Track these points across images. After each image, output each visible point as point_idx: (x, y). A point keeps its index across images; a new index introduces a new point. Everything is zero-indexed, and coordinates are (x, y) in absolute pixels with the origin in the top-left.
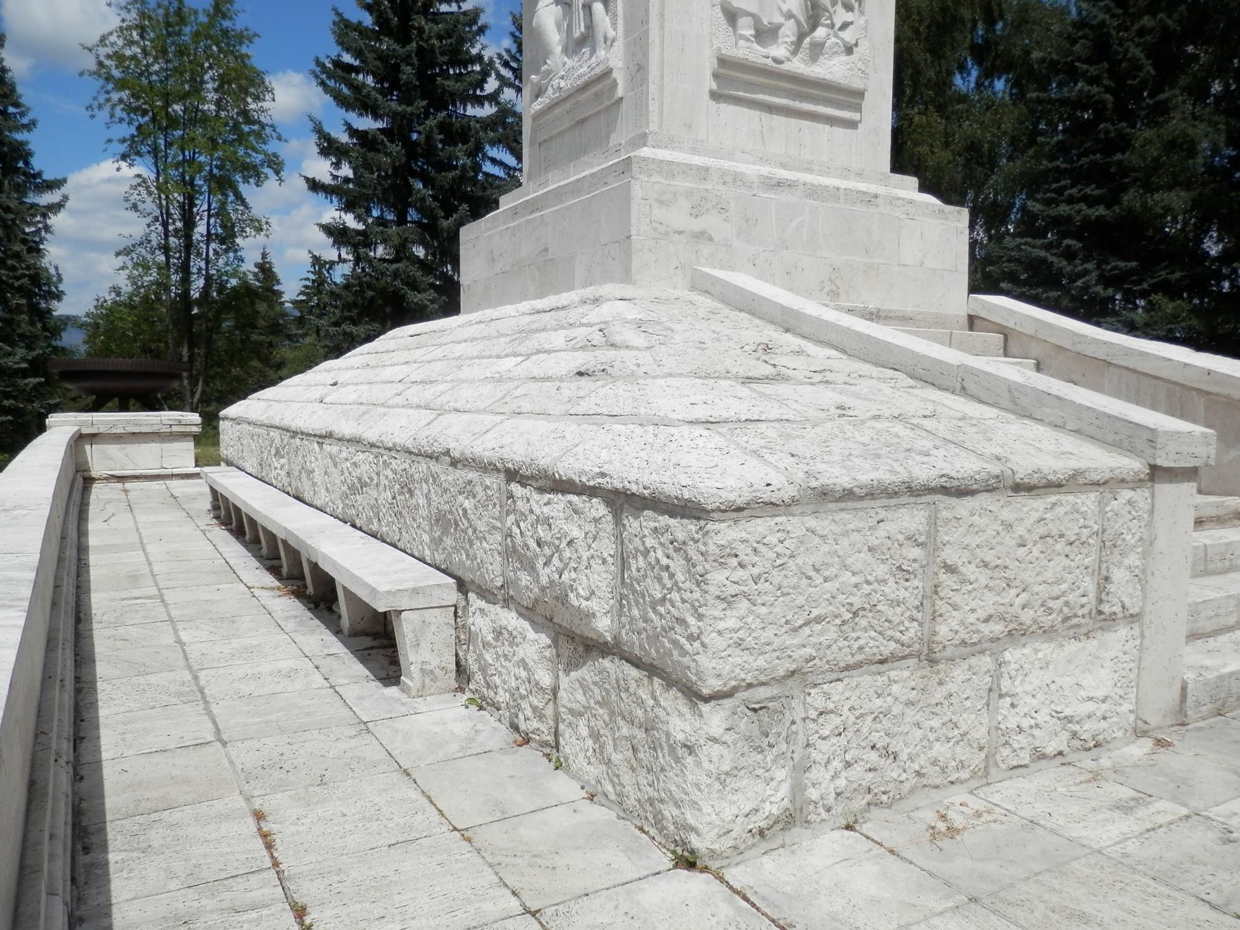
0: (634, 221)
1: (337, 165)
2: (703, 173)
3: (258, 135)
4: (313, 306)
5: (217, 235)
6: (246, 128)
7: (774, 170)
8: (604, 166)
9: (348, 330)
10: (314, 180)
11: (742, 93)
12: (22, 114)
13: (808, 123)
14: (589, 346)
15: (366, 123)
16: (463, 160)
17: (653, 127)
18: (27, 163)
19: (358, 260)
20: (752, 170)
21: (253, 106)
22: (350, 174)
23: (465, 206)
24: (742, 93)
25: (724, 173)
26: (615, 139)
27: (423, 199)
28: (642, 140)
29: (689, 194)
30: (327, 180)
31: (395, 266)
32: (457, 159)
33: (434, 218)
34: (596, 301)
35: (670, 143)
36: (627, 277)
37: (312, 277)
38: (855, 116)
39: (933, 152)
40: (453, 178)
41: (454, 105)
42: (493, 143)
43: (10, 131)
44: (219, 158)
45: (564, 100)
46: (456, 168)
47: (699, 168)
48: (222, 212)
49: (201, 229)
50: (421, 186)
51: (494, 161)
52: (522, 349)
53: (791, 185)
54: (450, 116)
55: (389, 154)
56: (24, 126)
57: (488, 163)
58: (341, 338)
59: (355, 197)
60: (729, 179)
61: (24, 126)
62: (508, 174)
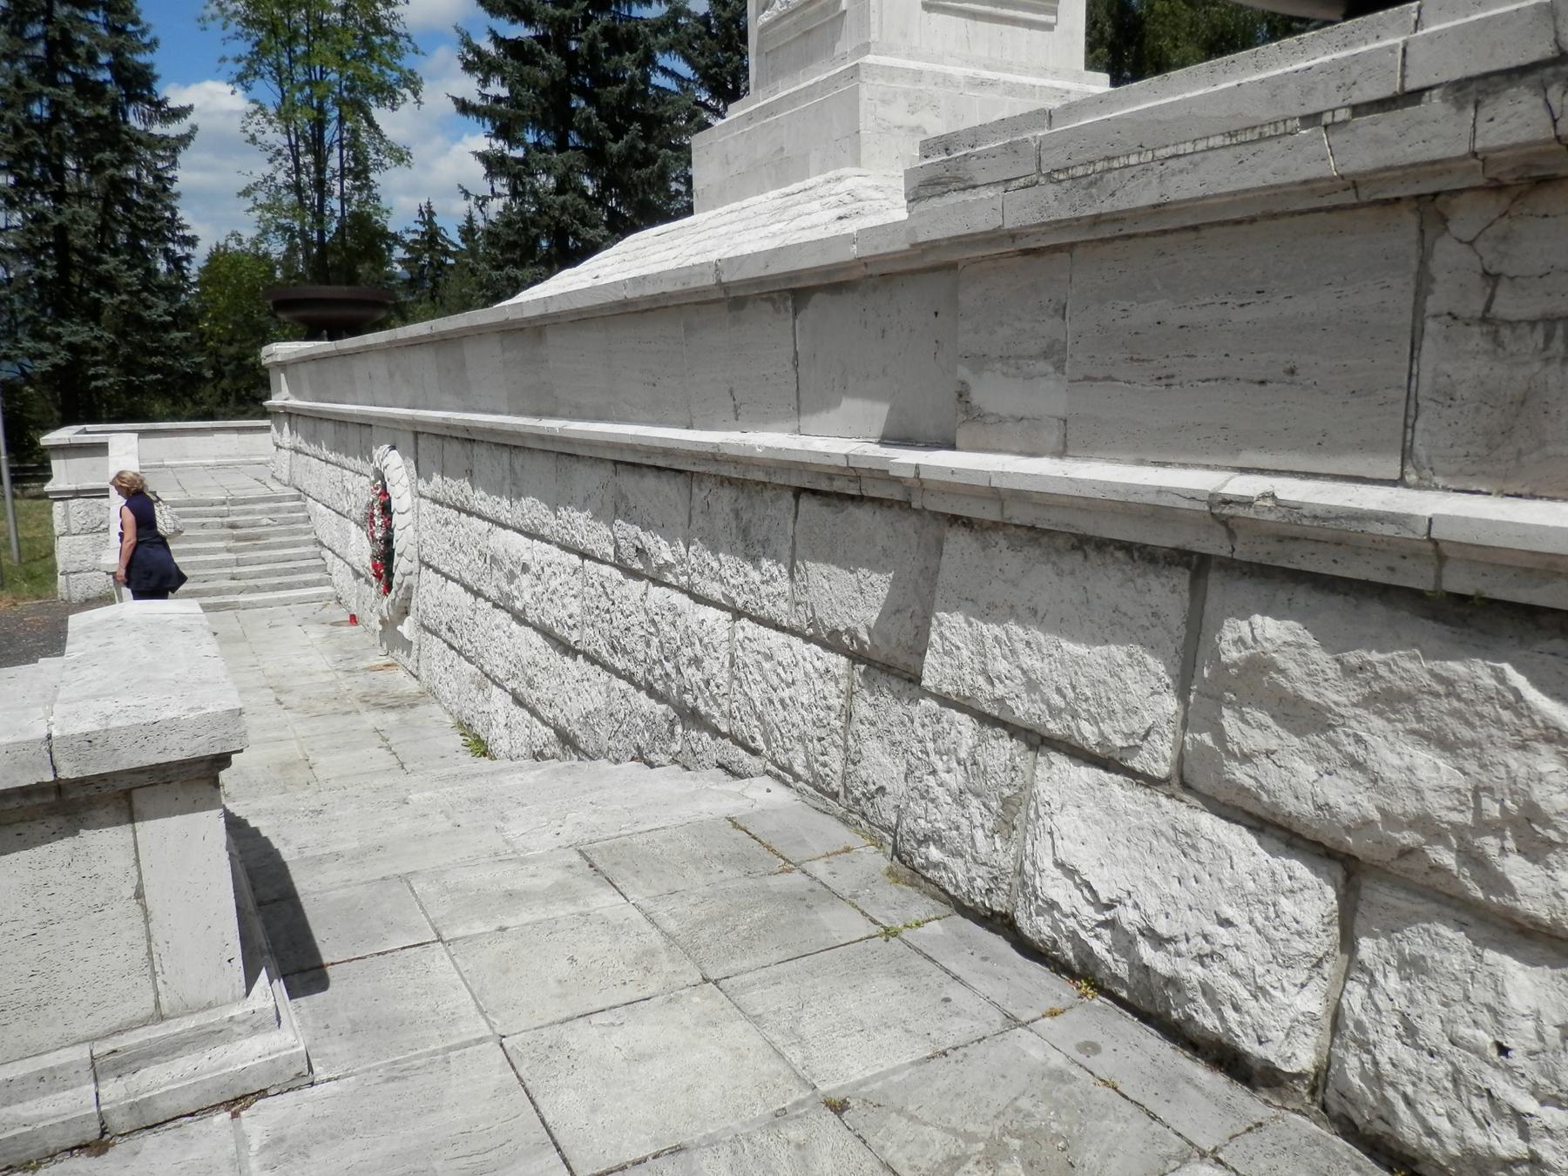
0: (862, 118)
1: (485, 82)
2: (918, 75)
3: (392, 48)
4: (424, 266)
5: (350, 169)
6: (377, 40)
7: (977, 71)
8: (832, 73)
9: (512, 275)
10: (463, 101)
11: (949, 3)
12: (143, 32)
13: (1009, 27)
14: (842, 203)
15: (518, 31)
16: (632, 71)
17: (874, 36)
18: (150, 90)
19: (515, 193)
20: (959, 71)
21: (383, 12)
22: (504, 92)
23: (637, 125)
24: (949, 3)
25: (935, 74)
26: (840, 47)
27: (588, 119)
28: (865, 48)
29: (906, 94)
30: (476, 100)
31: (562, 198)
32: (625, 70)
33: (601, 142)
34: (838, 179)
35: (889, 50)
36: (857, 162)
37: (421, 229)
38: (1052, 19)
39: (1176, 47)
40: (621, 94)
41: (618, 6)
42: (666, 49)
43: (131, 53)
44: (348, 78)
45: (792, 12)
46: (623, 80)
47: (914, 71)
48: (354, 144)
49: (334, 162)
50: (583, 103)
51: (665, 71)
52: (784, 217)
53: (993, 84)
54: (614, 19)
55: (546, 68)
56: (146, 46)
57: (659, 74)
58: (505, 283)
59: (510, 119)
60: (940, 80)
61: (146, 46)
62: (681, 87)
